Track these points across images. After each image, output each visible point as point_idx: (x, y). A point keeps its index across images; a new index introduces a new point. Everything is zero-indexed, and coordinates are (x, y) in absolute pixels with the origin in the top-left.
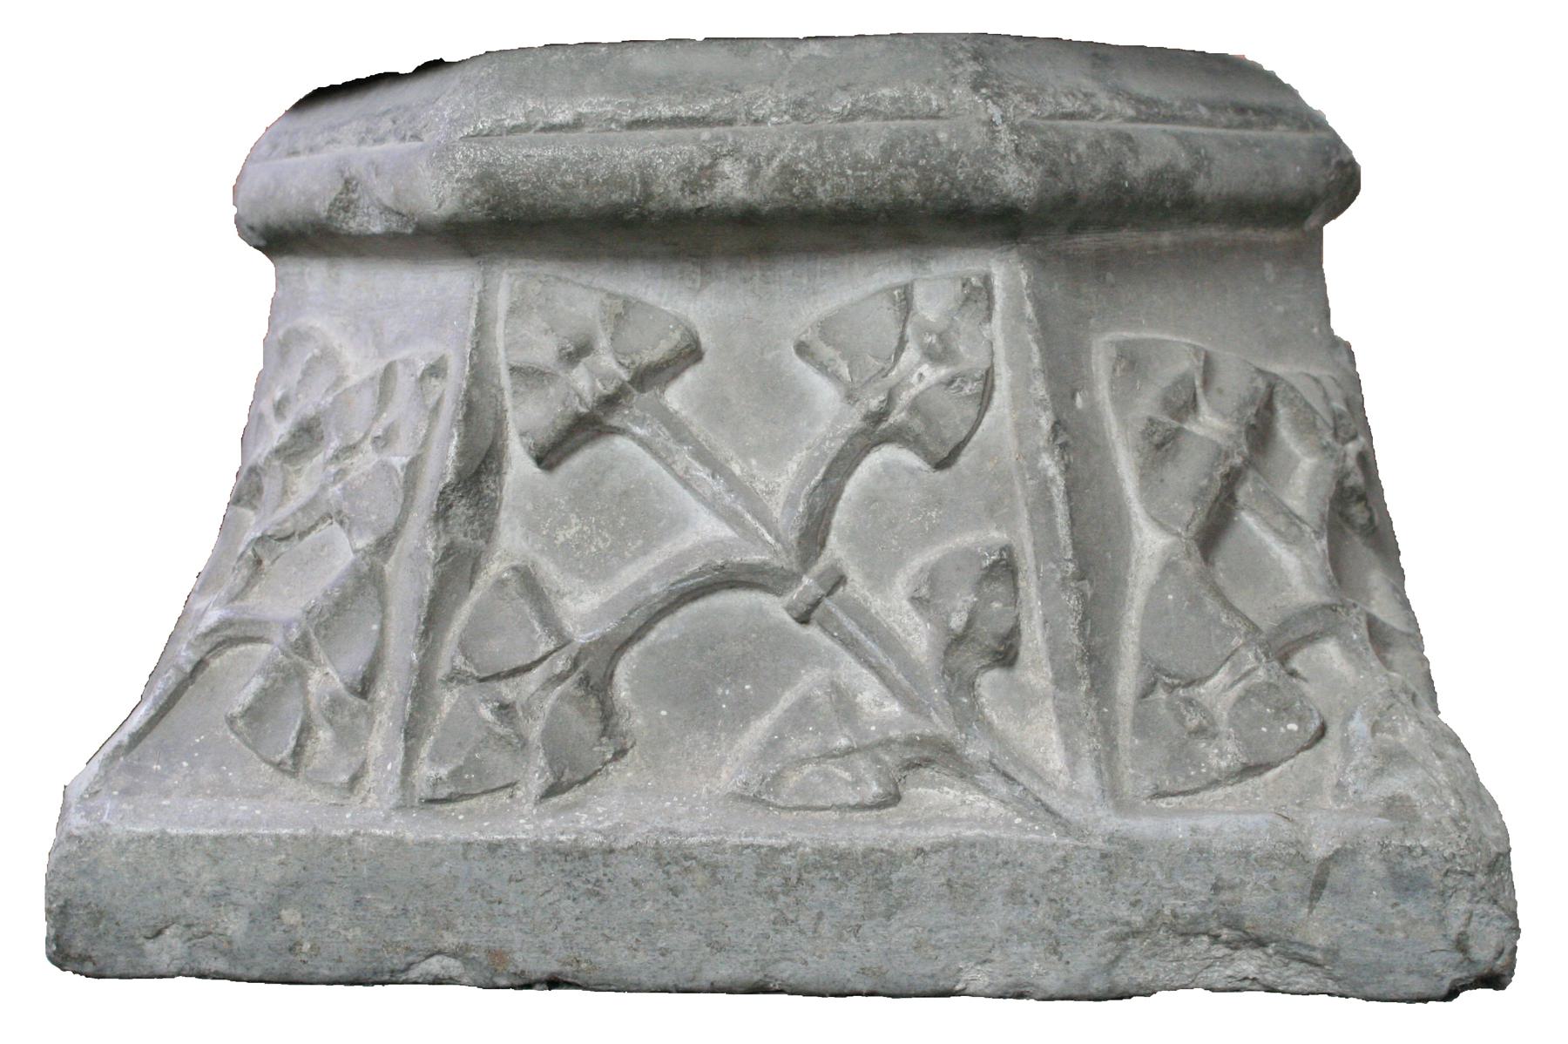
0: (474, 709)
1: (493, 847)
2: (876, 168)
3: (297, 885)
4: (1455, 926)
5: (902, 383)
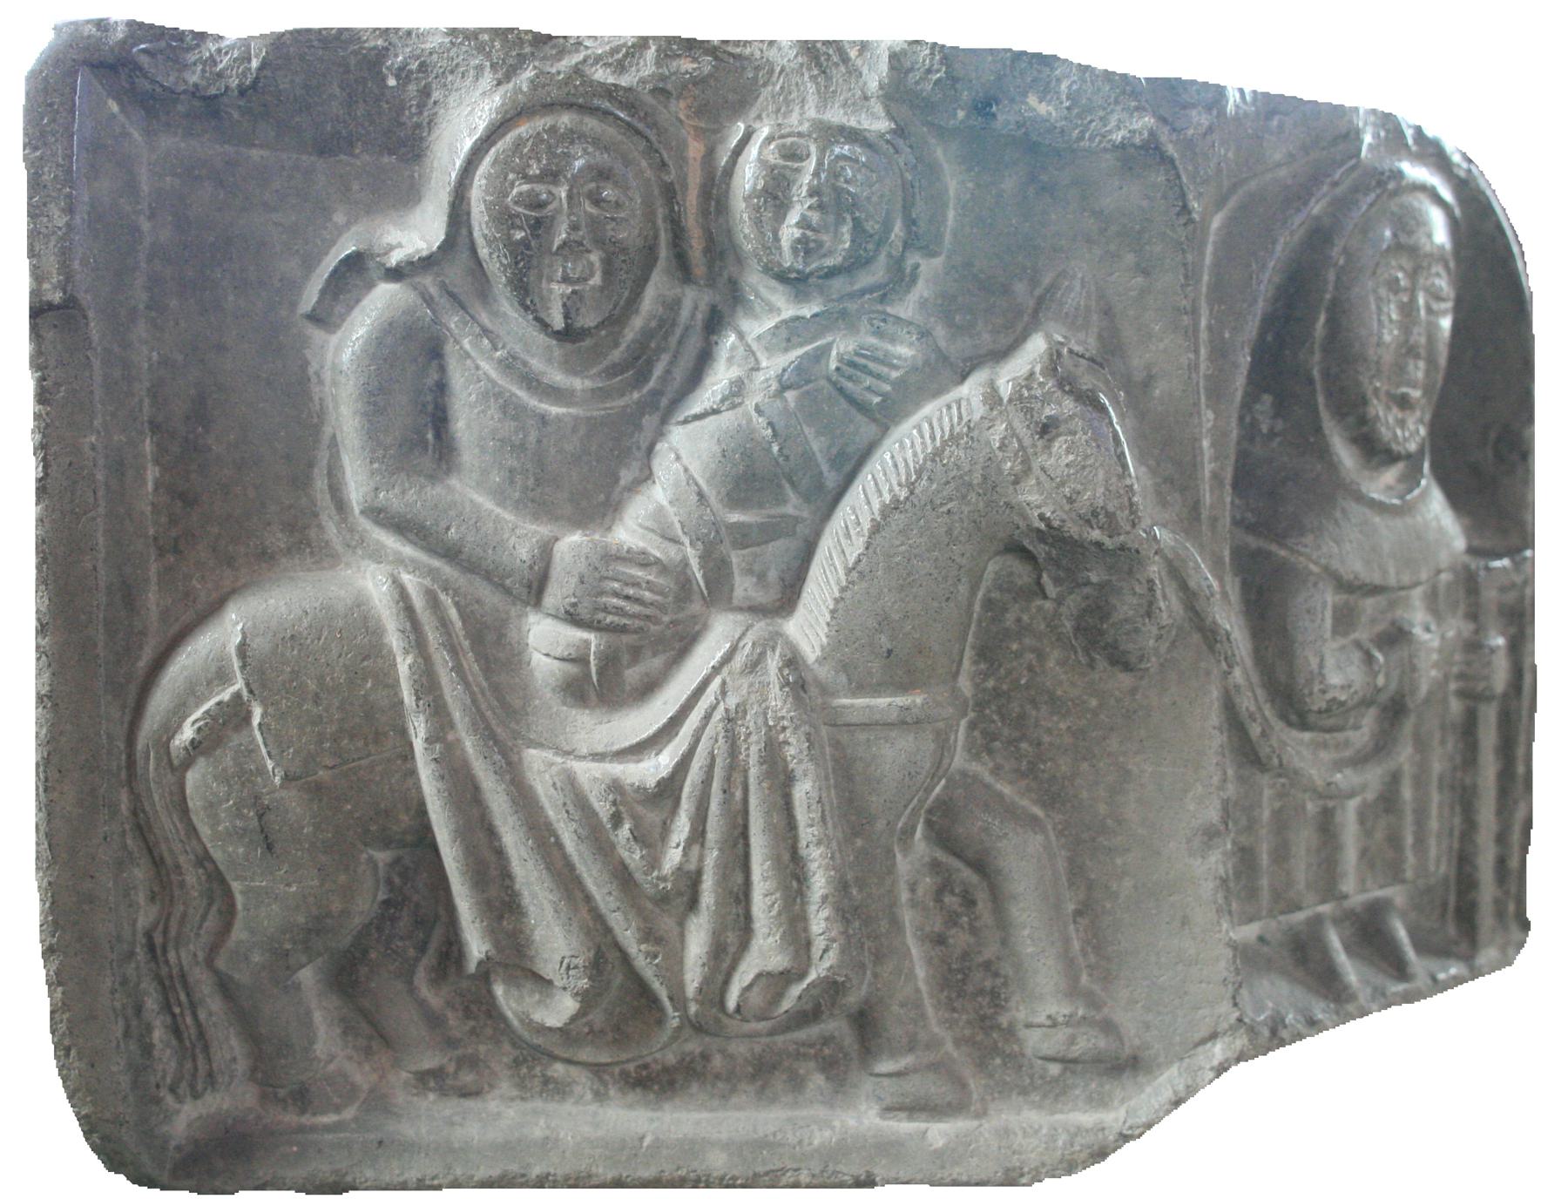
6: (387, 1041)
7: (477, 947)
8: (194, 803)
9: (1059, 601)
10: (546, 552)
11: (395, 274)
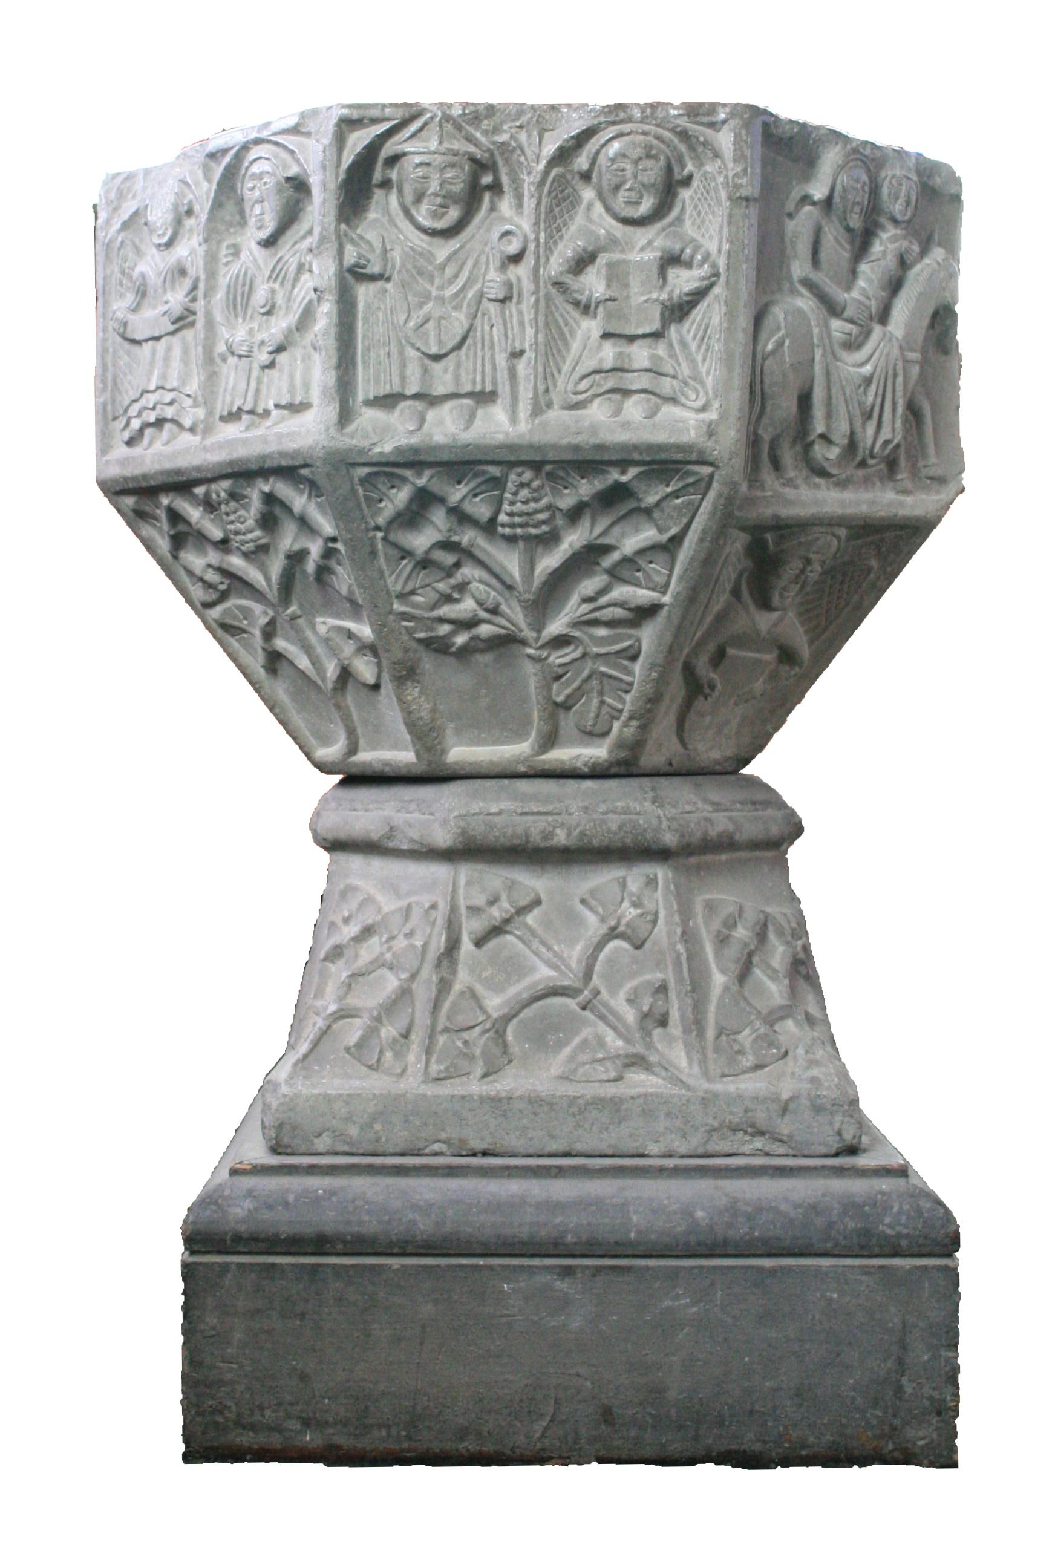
0: (453, 1042)
1: (463, 1097)
2: (615, 834)
3: (381, 1113)
4: (837, 1125)
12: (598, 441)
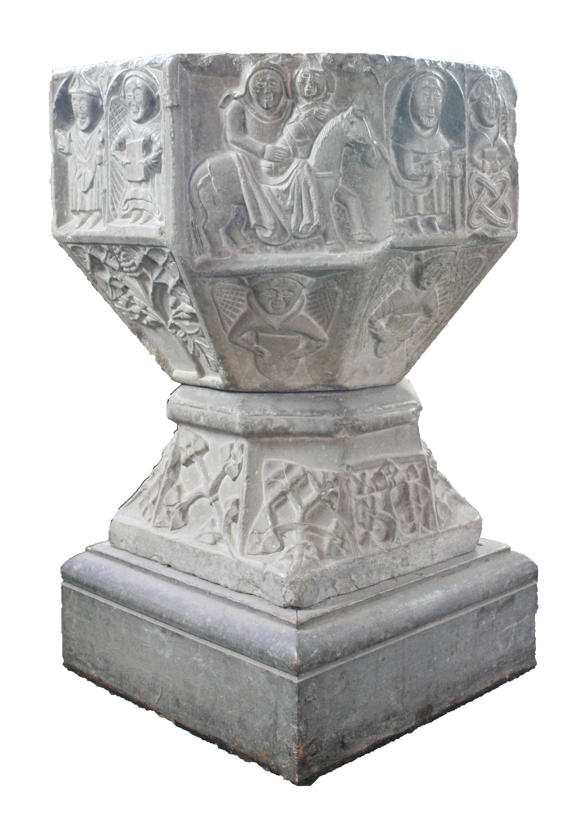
5: (229, 463)
6: (236, 243)
7: (253, 221)
8: (201, 196)
9: (358, 155)
10: (264, 148)
11: (236, 99)
12: (126, 236)
